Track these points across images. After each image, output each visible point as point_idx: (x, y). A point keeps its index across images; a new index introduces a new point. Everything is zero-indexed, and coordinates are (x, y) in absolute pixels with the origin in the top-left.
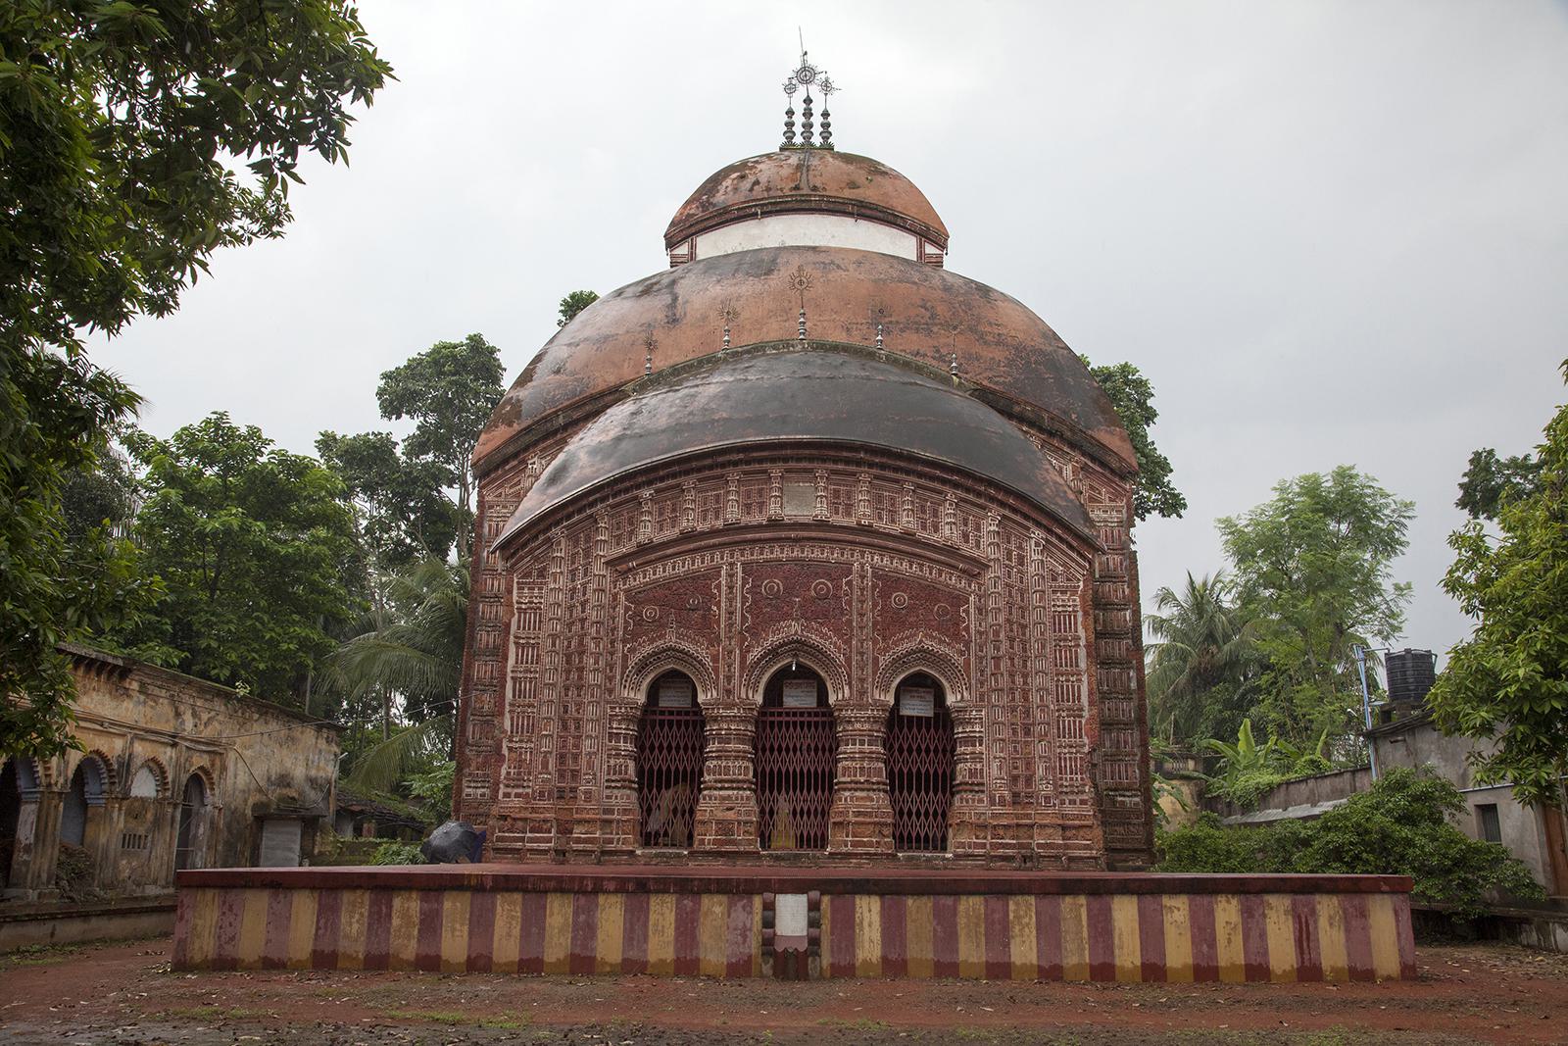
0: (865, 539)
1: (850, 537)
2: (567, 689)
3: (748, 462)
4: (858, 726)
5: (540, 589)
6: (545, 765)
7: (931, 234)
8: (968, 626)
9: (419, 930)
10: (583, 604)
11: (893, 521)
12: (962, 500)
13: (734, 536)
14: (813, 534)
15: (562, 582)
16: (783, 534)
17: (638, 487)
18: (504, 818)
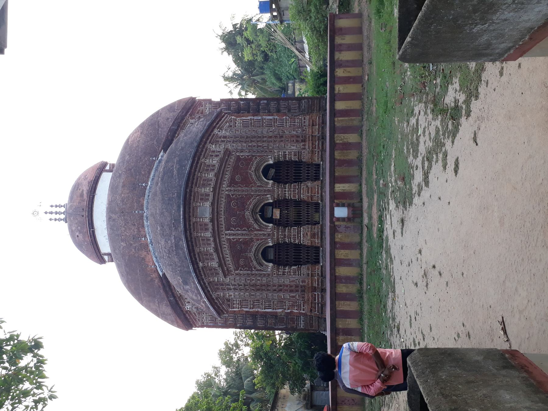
0: (217, 190)
1: (217, 194)
2: (268, 290)
3: (190, 229)
4: (280, 192)
6: (293, 297)
7: (102, 168)
10: (239, 285)
11: (211, 180)
12: (204, 156)
13: (217, 234)
14: (216, 207)
16: (216, 217)
17: (199, 267)
18: (311, 310)
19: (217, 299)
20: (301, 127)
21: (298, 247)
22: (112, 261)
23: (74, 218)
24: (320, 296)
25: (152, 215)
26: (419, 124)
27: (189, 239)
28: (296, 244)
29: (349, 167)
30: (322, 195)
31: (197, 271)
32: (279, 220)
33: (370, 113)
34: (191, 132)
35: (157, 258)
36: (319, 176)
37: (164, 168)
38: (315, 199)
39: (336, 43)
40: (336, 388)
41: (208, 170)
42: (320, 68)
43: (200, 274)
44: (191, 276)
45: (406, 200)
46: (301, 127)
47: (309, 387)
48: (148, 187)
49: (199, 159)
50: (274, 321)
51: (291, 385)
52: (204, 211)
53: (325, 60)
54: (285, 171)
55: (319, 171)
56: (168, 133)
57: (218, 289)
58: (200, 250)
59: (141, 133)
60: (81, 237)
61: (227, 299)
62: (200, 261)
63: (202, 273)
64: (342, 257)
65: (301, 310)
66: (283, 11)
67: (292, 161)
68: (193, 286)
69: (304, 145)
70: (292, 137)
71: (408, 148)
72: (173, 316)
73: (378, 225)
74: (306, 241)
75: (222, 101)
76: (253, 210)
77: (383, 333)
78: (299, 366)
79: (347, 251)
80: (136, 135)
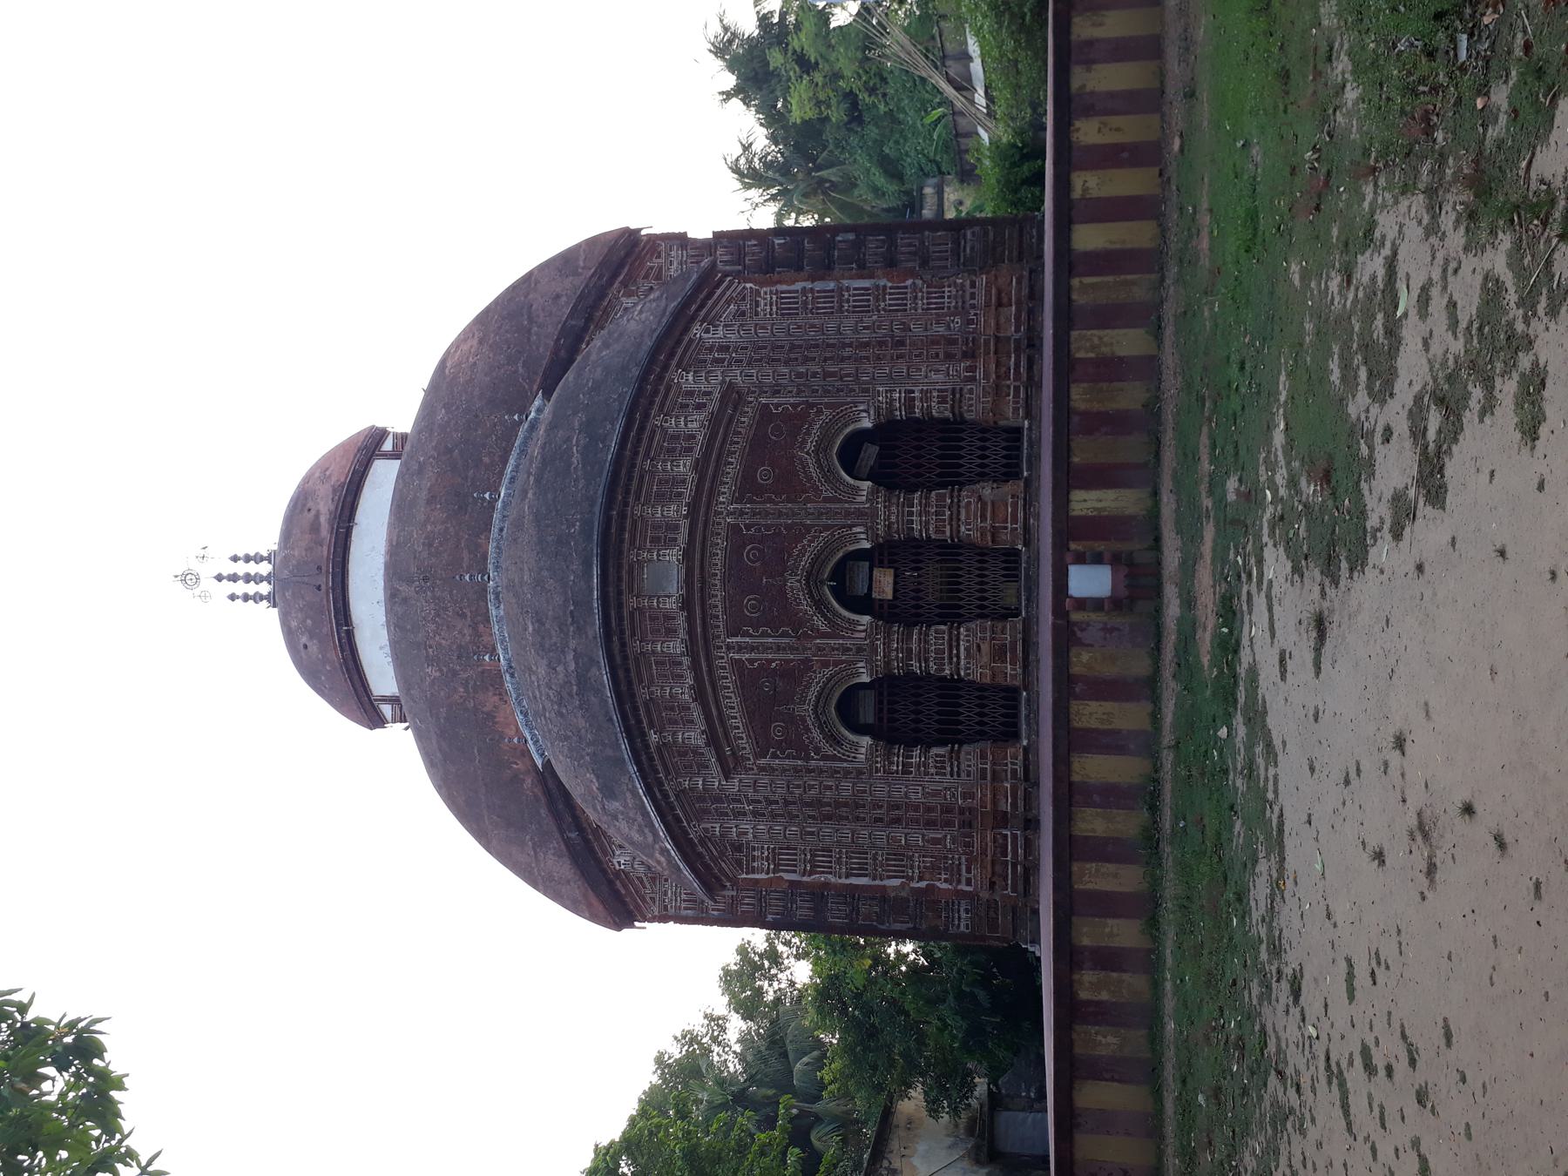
0: (703, 510)
2: (858, 819)
3: (622, 632)
4: (893, 518)
5: (754, 849)
6: (936, 841)
7: (370, 446)
10: (771, 803)
11: (684, 481)
13: (700, 646)
14: (697, 563)
15: (746, 826)
16: (697, 595)
17: (647, 746)
18: (992, 884)
19: (702, 842)
20: (961, 310)
21: (951, 688)
25: (511, 586)
26: (1401, 274)
27: (618, 660)
29: (1116, 433)
30: (1026, 528)
31: (644, 757)
32: (892, 604)
34: (621, 335)
35: (526, 715)
36: (1018, 466)
37: (543, 448)
38: (1005, 537)
39: (1073, 37)
41: (674, 449)
42: (1019, 133)
45: (1336, 547)
46: (961, 310)
47: (985, 1097)
48: (499, 504)
49: (646, 416)
50: (877, 909)
51: (931, 1089)
52: (664, 575)
53: (1037, 106)
54: (909, 452)
56: (558, 339)
57: (706, 812)
59: (481, 342)
60: (314, 648)
61: (732, 845)
62: (651, 725)
63: (657, 762)
64: (1094, 724)
65: (959, 882)
67: (932, 418)
68: (630, 802)
69: (972, 369)
70: (934, 342)
71: (1346, 366)
72: (577, 888)
73: (1218, 627)
74: (976, 669)
75: (719, 236)
76: (809, 574)
77: (1234, 983)
78: (954, 1037)
79: (1109, 706)
80: (465, 347)
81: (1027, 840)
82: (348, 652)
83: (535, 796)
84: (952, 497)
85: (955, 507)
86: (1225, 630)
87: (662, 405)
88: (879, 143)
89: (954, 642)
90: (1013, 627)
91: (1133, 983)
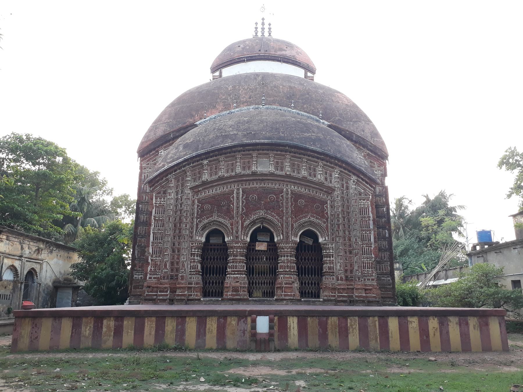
0: (288, 180)
1: (283, 179)
2: (174, 237)
3: (244, 151)
4: (286, 250)
5: (164, 198)
7: (309, 69)
8: (327, 212)
9: (114, 333)
10: (181, 205)
11: (299, 173)
12: (325, 165)
13: (239, 179)
14: (269, 178)
16: (257, 178)
17: (202, 160)
18: (149, 287)
19: (167, 179)
20: (363, 275)
21: (223, 272)
22: (213, 79)
23: (257, 42)
24: (165, 298)
25: (260, 112)
28: (226, 269)
30: (282, 300)
31: (198, 158)
32: (254, 249)
33: (388, 363)
34: (351, 151)
35: (214, 118)
36: (305, 297)
38: (279, 292)
39: (469, 318)
40: (52, 317)
41: (310, 169)
43: (195, 162)
44: (193, 151)
46: (363, 275)
47: (78, 284)
48: (290, 109)
49: (322, 160)
51: (81, 265)
52: (264, 166)
53: (429, 304)
54: (310, 256)
55: (312, 297)
56: (347, 131)
57: (178, 181)
58: (222, 161)
61: (166, 190)
62: (210, 161)
65: (150, 274)
66: (483, 256)
67: (323, 264)
69: (342, 279)
72: (153, 137)
75: (386, 189)
76: (265, 219)
79: (215, 332)
80: (344, 100)
81: (166, 300)
82: (237, 60)
83: (186, 123)
84: (294, 272)
85: (290, 273)
86: (243, 381)
87: (326, 165)
88: (412, 248)
89: (240, 272)
90: (245, 295)
91: (109, 341)
